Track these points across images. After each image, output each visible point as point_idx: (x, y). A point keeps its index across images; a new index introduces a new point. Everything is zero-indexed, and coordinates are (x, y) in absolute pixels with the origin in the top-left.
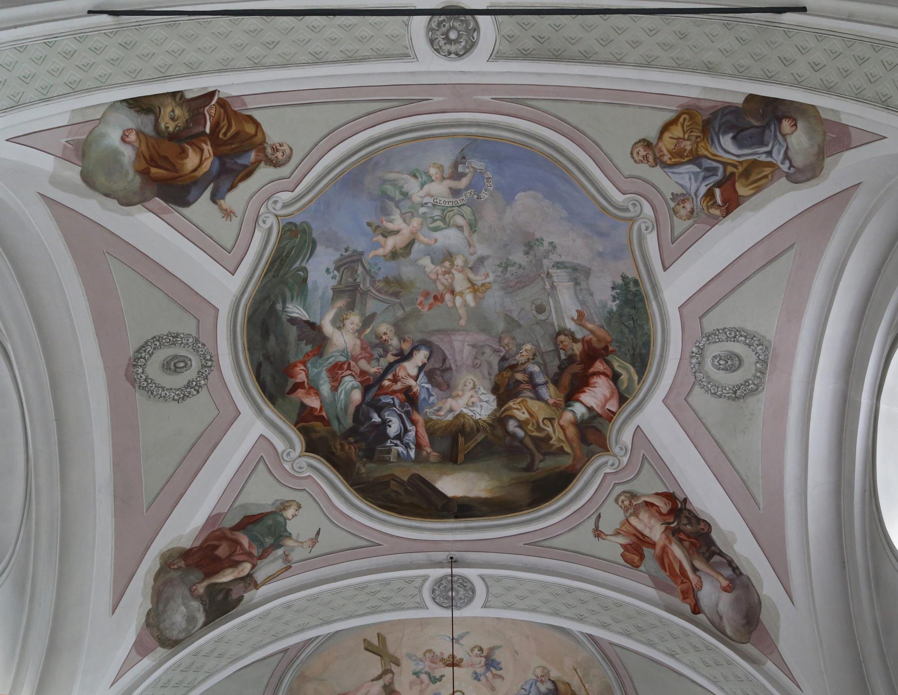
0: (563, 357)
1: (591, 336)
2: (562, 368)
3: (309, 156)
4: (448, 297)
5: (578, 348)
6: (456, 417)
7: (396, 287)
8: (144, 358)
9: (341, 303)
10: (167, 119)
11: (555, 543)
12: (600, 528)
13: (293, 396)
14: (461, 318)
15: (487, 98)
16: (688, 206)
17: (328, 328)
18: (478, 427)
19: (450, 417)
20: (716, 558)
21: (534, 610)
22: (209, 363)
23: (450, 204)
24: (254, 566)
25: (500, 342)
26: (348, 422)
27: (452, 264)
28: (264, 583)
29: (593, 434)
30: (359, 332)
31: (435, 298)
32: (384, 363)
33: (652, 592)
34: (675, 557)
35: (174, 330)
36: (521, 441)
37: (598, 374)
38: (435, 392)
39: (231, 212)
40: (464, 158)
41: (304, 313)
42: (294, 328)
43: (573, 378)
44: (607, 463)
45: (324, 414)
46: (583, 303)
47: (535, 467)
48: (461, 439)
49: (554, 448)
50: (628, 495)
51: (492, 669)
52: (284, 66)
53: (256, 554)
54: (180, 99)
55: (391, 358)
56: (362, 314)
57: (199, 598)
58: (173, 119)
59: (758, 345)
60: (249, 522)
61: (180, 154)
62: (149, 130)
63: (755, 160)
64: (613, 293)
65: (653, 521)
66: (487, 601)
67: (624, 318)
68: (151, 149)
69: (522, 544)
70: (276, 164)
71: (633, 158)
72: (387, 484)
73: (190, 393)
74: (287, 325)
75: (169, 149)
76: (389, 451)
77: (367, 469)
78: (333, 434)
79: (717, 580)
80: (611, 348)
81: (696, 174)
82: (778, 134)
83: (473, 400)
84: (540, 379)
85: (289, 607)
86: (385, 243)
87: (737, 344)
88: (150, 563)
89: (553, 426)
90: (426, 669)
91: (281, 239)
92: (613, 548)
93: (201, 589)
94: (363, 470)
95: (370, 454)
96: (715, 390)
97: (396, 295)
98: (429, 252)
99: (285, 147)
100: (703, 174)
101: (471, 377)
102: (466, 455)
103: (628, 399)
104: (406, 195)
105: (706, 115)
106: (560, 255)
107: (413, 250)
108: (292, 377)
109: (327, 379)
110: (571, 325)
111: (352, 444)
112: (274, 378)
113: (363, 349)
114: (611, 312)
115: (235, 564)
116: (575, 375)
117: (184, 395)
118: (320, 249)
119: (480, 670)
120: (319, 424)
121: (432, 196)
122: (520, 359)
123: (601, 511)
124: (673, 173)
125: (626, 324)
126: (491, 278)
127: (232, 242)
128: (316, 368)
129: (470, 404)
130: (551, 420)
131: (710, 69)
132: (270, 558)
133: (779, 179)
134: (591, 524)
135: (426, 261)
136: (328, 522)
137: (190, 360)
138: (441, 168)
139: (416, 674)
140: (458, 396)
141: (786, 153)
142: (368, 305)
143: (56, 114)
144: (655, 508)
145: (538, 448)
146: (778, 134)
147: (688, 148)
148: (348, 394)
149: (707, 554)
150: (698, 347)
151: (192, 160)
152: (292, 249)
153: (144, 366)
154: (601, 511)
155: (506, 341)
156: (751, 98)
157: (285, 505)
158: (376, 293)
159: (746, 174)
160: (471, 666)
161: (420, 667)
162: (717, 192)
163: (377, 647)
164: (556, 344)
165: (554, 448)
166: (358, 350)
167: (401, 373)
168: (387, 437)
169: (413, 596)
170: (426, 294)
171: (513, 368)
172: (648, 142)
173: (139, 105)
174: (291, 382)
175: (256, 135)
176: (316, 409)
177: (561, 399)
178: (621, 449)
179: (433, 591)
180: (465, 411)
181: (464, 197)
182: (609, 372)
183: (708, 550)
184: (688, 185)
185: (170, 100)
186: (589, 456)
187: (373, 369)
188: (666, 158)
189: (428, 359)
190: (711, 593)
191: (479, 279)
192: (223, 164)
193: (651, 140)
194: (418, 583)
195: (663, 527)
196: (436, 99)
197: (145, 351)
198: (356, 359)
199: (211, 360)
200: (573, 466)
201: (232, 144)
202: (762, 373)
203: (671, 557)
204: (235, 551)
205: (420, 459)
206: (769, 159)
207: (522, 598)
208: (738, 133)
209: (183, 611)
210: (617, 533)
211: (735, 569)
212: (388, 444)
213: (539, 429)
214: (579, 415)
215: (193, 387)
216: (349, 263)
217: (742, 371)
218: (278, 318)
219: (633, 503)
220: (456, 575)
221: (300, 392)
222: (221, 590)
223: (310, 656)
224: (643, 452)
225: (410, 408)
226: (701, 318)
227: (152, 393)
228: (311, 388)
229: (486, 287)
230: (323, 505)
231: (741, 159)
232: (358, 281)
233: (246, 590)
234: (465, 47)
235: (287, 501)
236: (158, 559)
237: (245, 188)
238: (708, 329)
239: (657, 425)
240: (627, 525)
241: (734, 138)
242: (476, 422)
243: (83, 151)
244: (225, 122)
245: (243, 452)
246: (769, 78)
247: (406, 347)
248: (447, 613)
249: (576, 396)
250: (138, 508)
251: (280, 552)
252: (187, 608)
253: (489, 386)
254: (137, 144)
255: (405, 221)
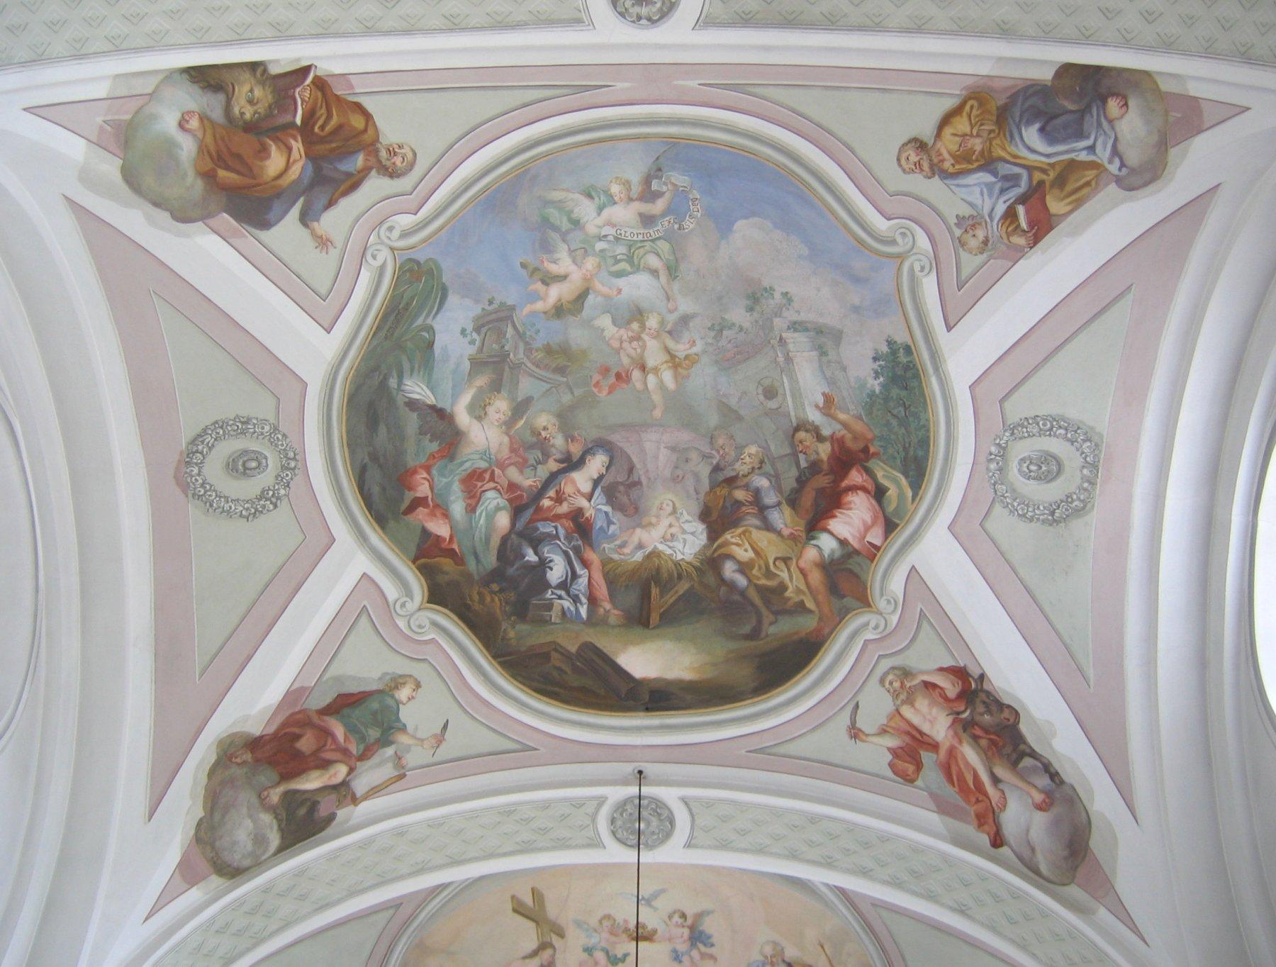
0: (803, 464)
1: (844, 432)
2: (802, 482)
3: (440, 162)
4: (636, 374)
5: (824, 451)
6: (649, 557)
7: (561, 359)
8: (201, 453)
9: (482, 381)
10: (243, 102)
11: (792, 749)
12: (858, 725)
13: (410, 518)
14: (655, 407)
15: (693, 84)
16: (981, 234)
17: (463, 418)
18: (679, 571)
19: (639, 557)
20: (1027, 762)
21: (761, 851)
22: (293, 464)
23: (640, 237)
24: (351, 770)
25: (711, 443)
26: (491, 561)
27: (643, 326)
28: (366, 797)
29: (847, 580)
30: (509, 424)
31: (618, 376)
32: (543, 472)
33: (934, 819)
34: (968, 764)
35: (244, 413)
36: (743, 593)
37: (854, 488)
38: (617, 517)
39: (328, 240)
40: (660, 170)
41: (428, 392)
42: (415, 415)
43: (820, 506)
44: (867, 624)
45: (455, 546)
46: (831, 382)
47: (763, 635)
48: (655, 591)
49: (791, 603)
50: (896, 672)
51: (700, 946)
52: (408, 32)
53: (355, 752)
54: (262, 75)
55: (553, 466)
56: (512, 399)
57: (272, 809)
58: (251, 102)
59: (1084, 441)
60: (345, 703)
61: (260, 152)
62: (217, 115)
63: (1072, 161)
64: (876, 366)
65: (934, 710)
66: (691, 837)
67: (892, 404)
68: (220, 142)
69: (743, 752)
70: (393, 174)
71: (900, 165)
72: (546, 657)
73: (264, 507)
74: (404, 411)
75: (243, 143)
76: (549, 607)
77: (516, 633)
78: (469, 576)
79: (1028, 793)
80: (872, 450)
81: (990, 186)
82: (1103, 119)
83: (673, 530)
84: (770, 498)
85: (401, 834)
86: (547, 294)
87: (1054, 440)
88: (203, 753)
89: (789, 570)
90: (603, 944)
91: (398, 282)
92: (876, 754)
93: (275, 795)
94: (512, 634)
95: (521, 611)
96: (1025, 511)
97: (561, 370)
98: (610, 308)
99: (406, 150)
100: (999, 185)
101: (670, 496)
102: (662, 615)
103: (896, 526)
104: (576, 223)
105: (1002, 100)
106: (798, 312)
107: (586, 304)
108: (410, 489)
109: (460, 494)
110: (814, 416)
111: (495, 593)
112: (385, 493)
113: (513, 450)
114: (872, 395)
115: (325, 765)
116: (821, 492)
117: (256, 510)
118: (453, 300)
119: (682, 947)
120: (448, 561)
121: (614, 226)
122: (741, 468)
123: (860, 698)
124: (958, 186)
125: (895, 412)
126: (698, 348)
127: (329, 283)
128: (444, 476)
129: (669, 536)
130: (786, 560)
131: (1005, 32)
132: (376, 759)
133: (1107, 185)
134: (845, 719)
135: (605, 322)
136: (460, 712)
137: (266, 458)
138: (627, 184)
139: (589, 950)
140: (650, 524)
141: (1114, 146)
142: (521, 386)
143: (91, 79)
144: (938, 690)
145: (767, 602)
146: (1103, 119)
147: (978, 148)
148: (491, 517)
149: (1014, 756)
150: (999, 445)
151: (275, 162)
152: (412, 298)
153: (200, 465)
154: (860, 698)
155: (720, 441)
156: (1067, 70)
157: (397, 682)
158: (533, 368)
159: (1060, 181)
160: (670, 940)
161: (594, 940)
162: (1021, 210)
163: (530, 909)
164: (792, 445)
165: (791, 603)
166: (505, 453)
167: (568, 489)
168: (547, 585)
169: (582, 828)
170: (605, 371)
171: (731, 481)
172: (921, 142)
173: (207, 78)
174: (409, 497)
175: (365, 130)
176: (444, 539)
177: (800, 527)
178: (889, 602)
179: (613, 821)
180: (661, 547)
181: (659, 227)
182: (870, 486)
183: (1014, 750)
184: (979, 202)
185: (247, 75)
186: (842, 615)
187: (528, 481)
188: (947, 165)
189: (607, 469)
190: (1020, 814)
191: (681, 349)
192: (318, 170)
193: (925, 140)
194: (590, 808)
195: (950, 719)
196: (619, 85)
197: (202, 442)
198: (503, 467)
199: (294, 459)
200: (818, 630)
201: (331, 142)
202: (1090, 483)
203: (960, 762)
204: (325, 745)
205: (594, 621)
206: (1092, 158)
207: (743, 833)
208: (1046, 123)
209: (249, 826)
210: (883, 731)
211: (1054, 776)
212: (549, 595)
213: (769, 574)
214: (826, 553)
215: (268, 499)
216: (494, 321)
217: (1062, 478)
218: (391, 401)
219: (906, 684)
220: (646, 797)
221: (421, 512)
222: (306, 800)
223: (433, 916)
224: (920, 606)
225: (580, 542)
226: (1002, 401)
227: (211, 506)
228: (437, 506)
229: (691, 360)
230: (451, 683)
231: (1052, 160)
232: (506, 348)
233: (340, 803)
234: (661, 10)
235: (401, 676)
236: (214, 747)
237: (350, 205)
238: (1013, 418)
239: (948, 577)
240: (898, 718)
241: (1042, 130)
242: (677, 564)
243: (126, 136)
244: (323, 111)
245: (337, 605)
246: (1086, 38)
247: (576, 450)
248: (629, 856)
249: (821, 524)
250: (189, 674)
251: (390, 751)
252: (255, 821)
253: (696, 508)
254: (200, 134)
255: (574, 262)
